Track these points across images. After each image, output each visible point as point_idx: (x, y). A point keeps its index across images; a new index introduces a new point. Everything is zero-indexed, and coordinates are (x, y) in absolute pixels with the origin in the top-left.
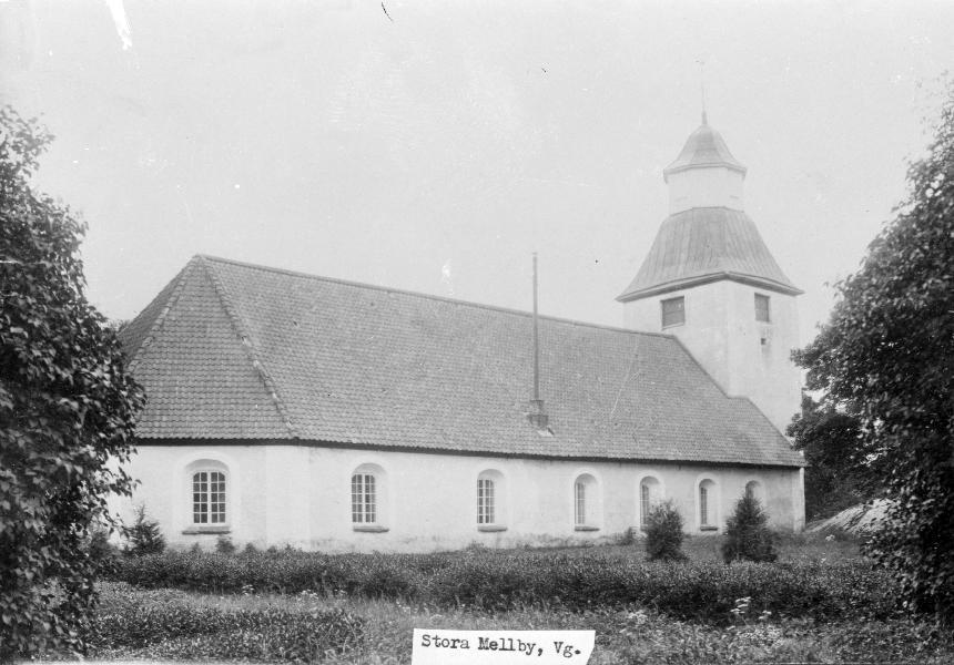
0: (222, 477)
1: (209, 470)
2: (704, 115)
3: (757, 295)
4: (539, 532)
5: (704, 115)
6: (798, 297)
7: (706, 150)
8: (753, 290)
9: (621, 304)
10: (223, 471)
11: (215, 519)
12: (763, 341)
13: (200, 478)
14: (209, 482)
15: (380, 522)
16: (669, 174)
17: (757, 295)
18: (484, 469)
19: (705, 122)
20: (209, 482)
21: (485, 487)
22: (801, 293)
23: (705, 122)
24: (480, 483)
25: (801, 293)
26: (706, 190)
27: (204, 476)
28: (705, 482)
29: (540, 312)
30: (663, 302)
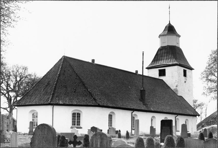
0: (79, 114)
1: (76, 112)
2: (170, 21)
3: (184, 70)
4: (98, 128)
5: (170, 21)
6: (193, 70)
7: (170, 30)
8: (183, 68)
9: (147, 69)
10: (80, 113)
11: (77, 125)
12: (185, 82)
13: (74, 114)
14: (76, 115)
15: (81, 126)
16: (160, 36)
17: (184, 70)
18: (112, 111)
19: (170, 22)
20: (76, 115)
21: (110, 117)
22: (194, 69)
23: (170, 22)
24: (109, 115)
25: (194, 69)
26: (170, 41)
27: (75, 113)
28: (153, 117)
29: (144, 75)
30: (159, 70)
